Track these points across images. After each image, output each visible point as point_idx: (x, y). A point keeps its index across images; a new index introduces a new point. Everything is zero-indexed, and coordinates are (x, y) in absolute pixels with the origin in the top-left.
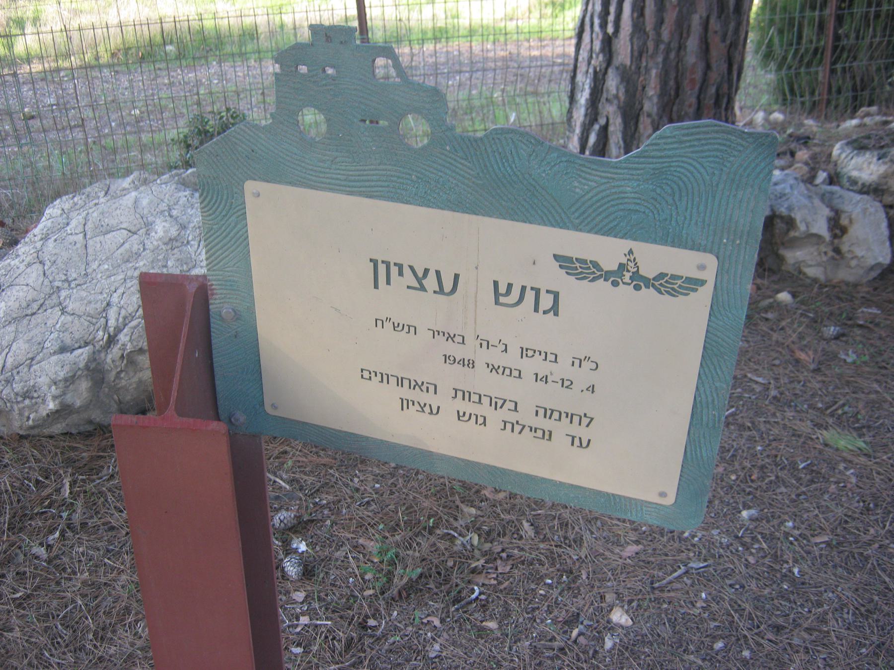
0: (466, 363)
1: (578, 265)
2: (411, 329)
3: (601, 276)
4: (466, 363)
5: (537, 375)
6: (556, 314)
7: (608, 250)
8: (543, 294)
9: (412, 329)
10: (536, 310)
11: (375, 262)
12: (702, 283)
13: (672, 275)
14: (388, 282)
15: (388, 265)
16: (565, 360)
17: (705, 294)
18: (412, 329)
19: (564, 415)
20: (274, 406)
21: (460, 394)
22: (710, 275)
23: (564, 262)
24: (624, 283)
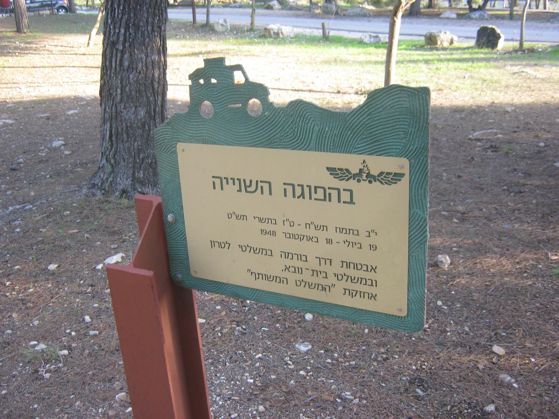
0: (272, 233)
1: (339, 172)
2: (243, 217)
3: (351, 178)
4: (272, 233)
7: (352, 162)
8: (296, 187)
9: (325, 228)
10: (294, 197)
12: (402, 175)
13: (387, 173)
15: (302, 186)
16: (332, 229)
17: (405, 180)
18: (325, 228)
20: (196, 272)
24: (363, 180)
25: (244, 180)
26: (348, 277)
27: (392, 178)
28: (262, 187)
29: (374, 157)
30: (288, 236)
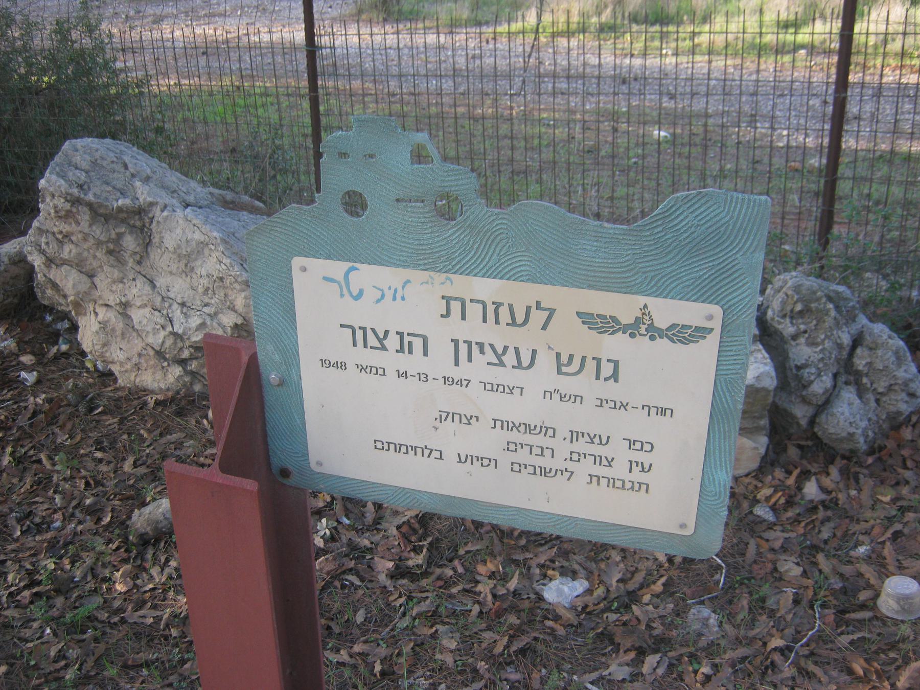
1: (599, 320)
2: (342, 366)
3: (619, 329)
6: (616, 381)
7: (624, 306)
9: (578, 399)
10: (598, 378)
11: (456, 342)
14: (470, 360)
15: (577, 433)
18: (578, 399)
19: (410, 448)
20: (319, 464)
22: (717, 324)
23: (587, 319)
24: (640, 335)
27: (682, 335)
29: (660, 301)
30: (489, 387)
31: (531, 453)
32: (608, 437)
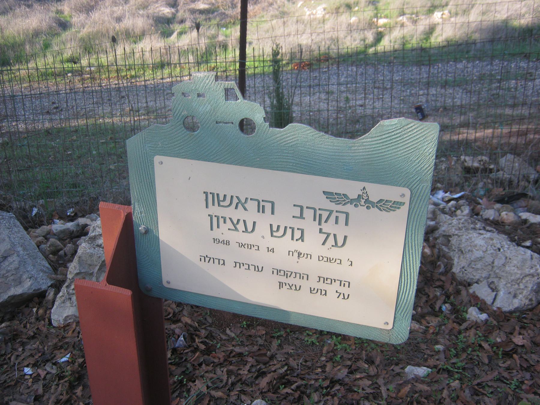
0: (225, 242)
1: (336, 196)
4: (225, 242)
5: (268, 248)
6: (303, 241)
9: (309, 256)
10: (292, 239)
14: (218, 227)
15: (213, 194)
17: (405, 209)
18: (309, 256)
20: (169, 283)
21: (238, 265)
22: (407, 200)
25: (218, 195)
26: (340, 294)
27: (383, 205)
28: (337, 218)
31: (219, 264)
32: (262, 267)
